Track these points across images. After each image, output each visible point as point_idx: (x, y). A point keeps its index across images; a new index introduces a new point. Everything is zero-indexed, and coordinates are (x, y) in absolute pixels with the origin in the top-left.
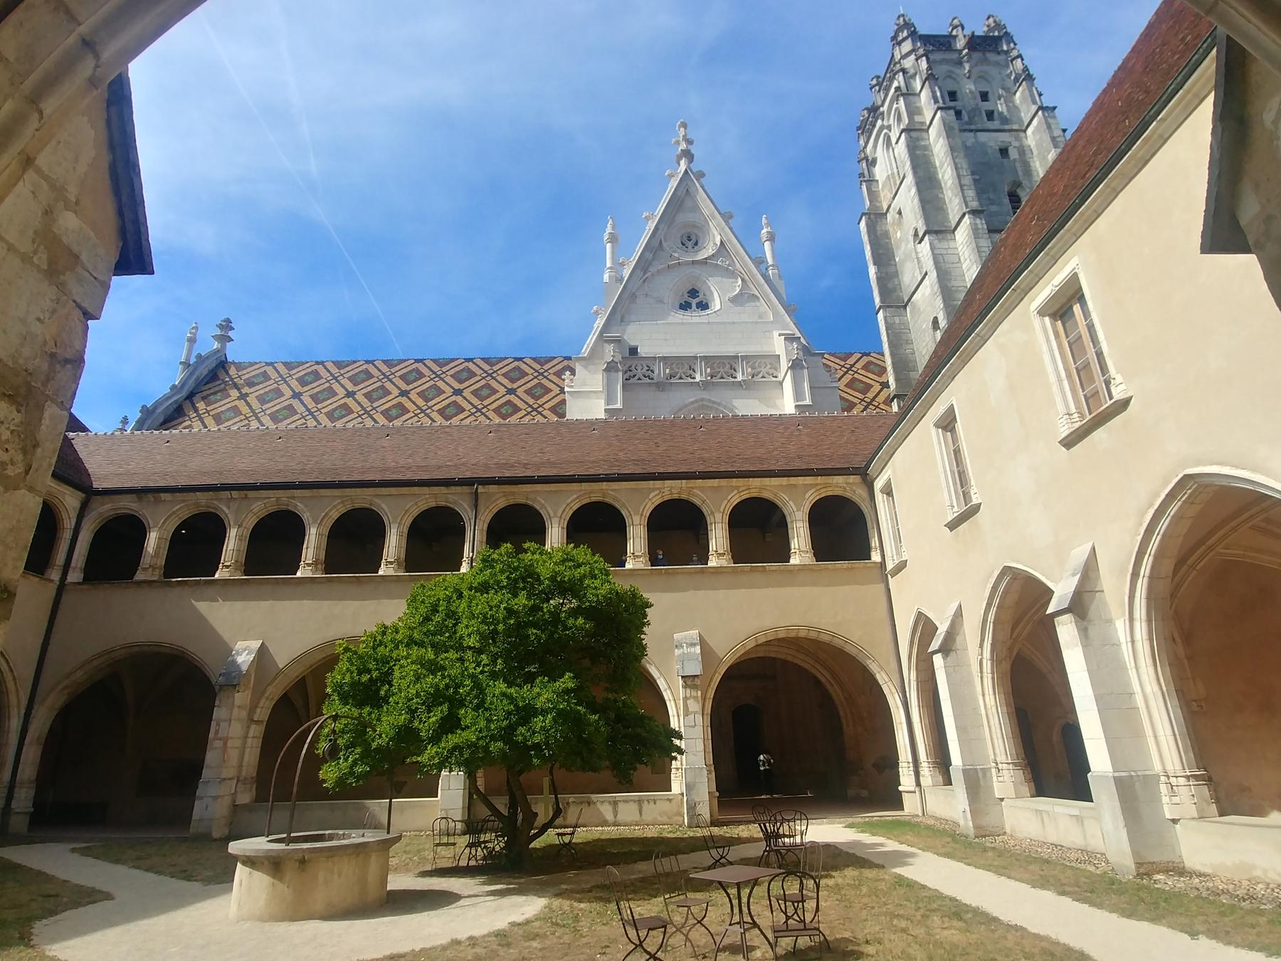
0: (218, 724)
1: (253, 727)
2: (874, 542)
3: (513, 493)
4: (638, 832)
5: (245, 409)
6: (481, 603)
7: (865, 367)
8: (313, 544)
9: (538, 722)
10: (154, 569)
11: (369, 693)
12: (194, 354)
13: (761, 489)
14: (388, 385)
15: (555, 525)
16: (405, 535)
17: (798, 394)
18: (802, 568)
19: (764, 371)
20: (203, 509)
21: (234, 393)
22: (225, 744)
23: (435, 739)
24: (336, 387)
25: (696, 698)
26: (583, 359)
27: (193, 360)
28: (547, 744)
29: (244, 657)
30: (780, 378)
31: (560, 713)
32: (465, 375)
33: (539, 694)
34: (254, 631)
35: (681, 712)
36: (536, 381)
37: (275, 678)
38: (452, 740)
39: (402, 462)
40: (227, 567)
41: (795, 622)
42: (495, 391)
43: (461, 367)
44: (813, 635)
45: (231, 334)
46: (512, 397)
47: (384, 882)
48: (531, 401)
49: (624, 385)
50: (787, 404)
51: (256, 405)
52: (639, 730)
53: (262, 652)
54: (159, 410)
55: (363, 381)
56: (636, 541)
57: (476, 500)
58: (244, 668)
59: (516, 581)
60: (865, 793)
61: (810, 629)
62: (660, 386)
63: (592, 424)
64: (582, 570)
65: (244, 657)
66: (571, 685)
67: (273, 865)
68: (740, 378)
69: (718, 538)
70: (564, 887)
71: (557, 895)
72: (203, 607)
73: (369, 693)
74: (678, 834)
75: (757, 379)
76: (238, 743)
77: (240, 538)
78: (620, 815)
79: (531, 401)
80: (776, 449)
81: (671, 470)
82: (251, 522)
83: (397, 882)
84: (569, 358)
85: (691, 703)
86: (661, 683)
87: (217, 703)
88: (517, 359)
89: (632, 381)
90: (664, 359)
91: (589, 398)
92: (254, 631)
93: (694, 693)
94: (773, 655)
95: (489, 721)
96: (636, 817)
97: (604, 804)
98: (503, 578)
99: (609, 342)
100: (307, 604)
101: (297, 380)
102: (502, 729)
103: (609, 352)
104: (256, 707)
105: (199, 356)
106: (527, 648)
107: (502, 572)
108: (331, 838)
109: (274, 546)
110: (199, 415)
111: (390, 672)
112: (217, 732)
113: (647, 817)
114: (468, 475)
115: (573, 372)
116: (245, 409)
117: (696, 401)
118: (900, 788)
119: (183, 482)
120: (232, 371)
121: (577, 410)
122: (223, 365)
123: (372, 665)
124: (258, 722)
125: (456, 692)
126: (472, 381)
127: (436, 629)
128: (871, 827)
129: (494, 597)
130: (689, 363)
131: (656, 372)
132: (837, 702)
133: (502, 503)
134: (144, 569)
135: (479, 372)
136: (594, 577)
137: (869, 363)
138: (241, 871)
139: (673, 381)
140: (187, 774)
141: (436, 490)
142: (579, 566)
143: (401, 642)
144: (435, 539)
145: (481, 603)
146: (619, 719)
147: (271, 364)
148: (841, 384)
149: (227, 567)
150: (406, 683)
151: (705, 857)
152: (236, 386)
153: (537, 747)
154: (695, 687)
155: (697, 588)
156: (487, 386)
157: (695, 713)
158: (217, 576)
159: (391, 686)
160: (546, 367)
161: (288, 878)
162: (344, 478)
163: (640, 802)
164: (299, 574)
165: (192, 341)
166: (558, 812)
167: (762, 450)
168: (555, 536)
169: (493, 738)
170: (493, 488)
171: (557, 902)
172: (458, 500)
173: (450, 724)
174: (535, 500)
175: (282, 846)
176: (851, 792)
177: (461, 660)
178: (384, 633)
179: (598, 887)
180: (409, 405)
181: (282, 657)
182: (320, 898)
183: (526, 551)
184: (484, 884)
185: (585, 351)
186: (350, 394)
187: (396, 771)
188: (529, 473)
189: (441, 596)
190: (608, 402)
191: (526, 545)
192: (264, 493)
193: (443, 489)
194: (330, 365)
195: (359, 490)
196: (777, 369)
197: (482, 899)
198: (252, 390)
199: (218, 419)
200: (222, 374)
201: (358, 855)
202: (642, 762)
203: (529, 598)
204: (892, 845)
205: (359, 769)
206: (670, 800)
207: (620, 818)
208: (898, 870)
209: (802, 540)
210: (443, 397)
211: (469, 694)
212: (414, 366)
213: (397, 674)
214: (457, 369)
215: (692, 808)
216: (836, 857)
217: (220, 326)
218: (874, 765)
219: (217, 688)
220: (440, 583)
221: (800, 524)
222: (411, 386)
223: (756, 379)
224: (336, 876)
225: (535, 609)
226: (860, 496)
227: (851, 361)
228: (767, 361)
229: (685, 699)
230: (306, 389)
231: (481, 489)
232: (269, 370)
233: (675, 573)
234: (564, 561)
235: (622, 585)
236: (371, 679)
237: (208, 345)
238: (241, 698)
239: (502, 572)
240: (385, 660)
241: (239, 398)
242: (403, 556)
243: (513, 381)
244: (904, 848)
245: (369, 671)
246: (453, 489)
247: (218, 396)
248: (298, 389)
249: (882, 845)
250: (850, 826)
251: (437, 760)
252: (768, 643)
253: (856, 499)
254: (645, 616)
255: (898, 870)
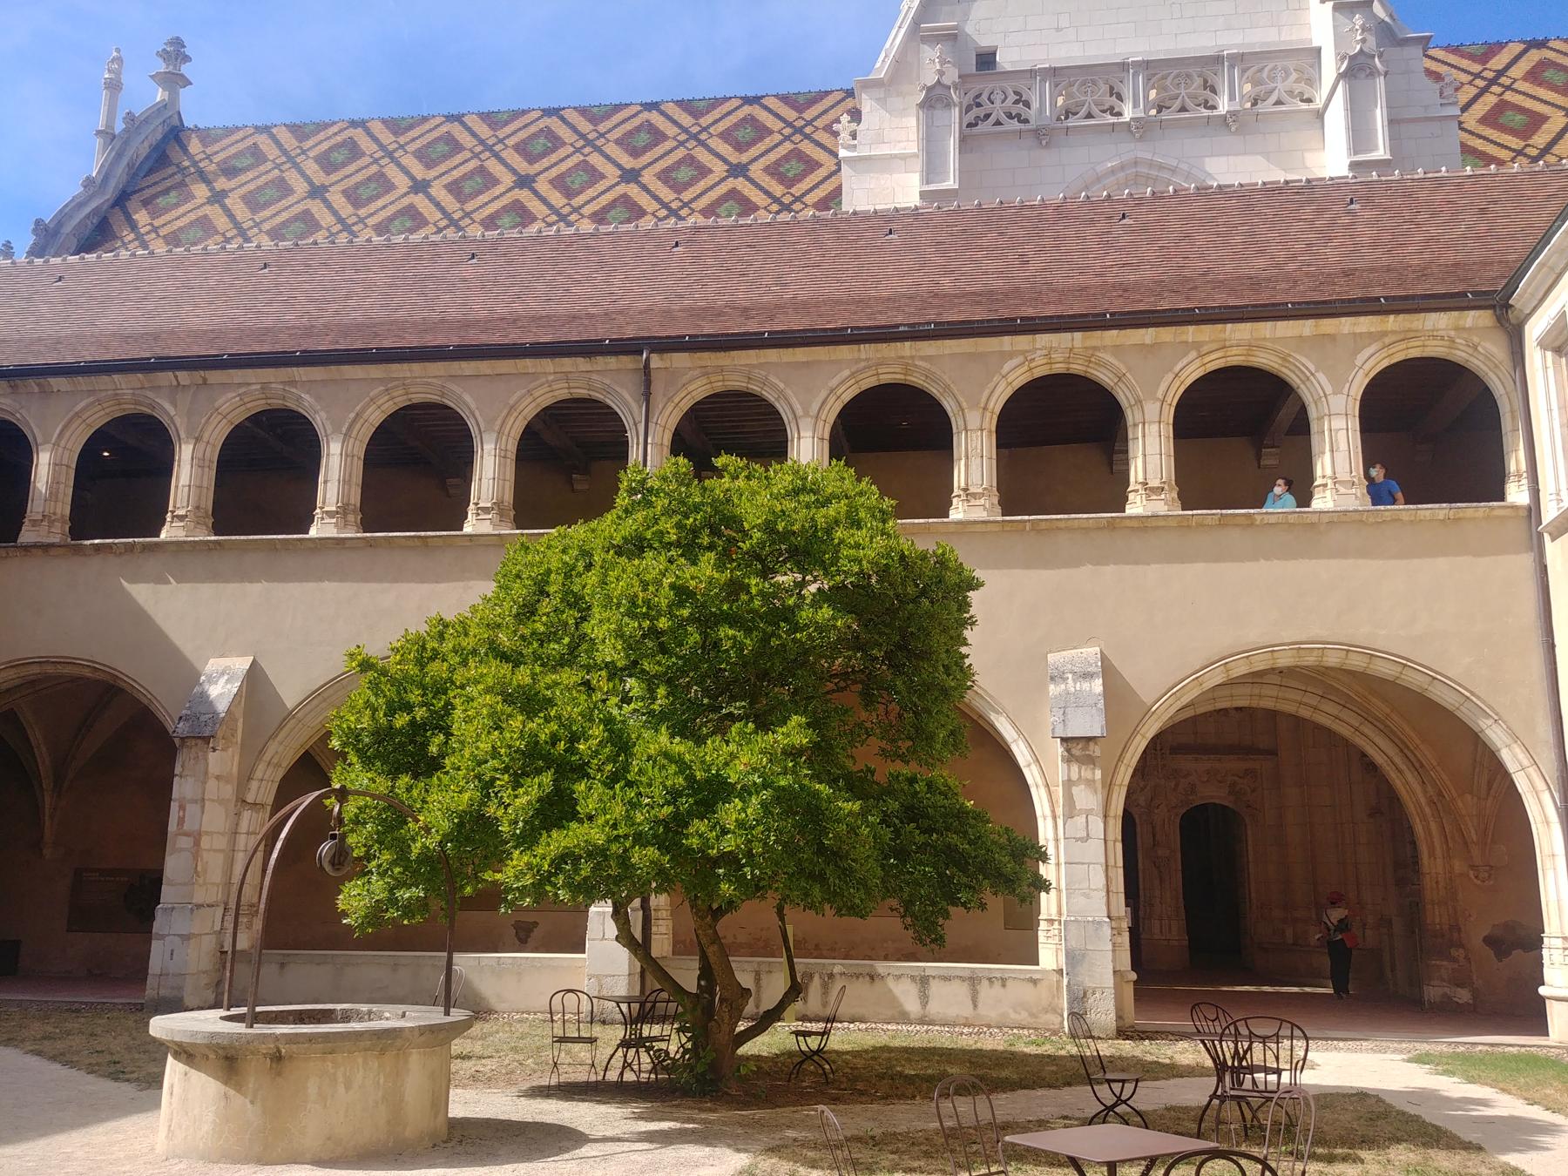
0: (182, 808)
1: (247, 814)
2: (1516, 461)
3: (721, 370)
4: (966, 1040)
5: (222, 222)
6: (624, 579)
7: (1534, 75)
8: (337, 474)
9: (730, 812)
10: (51, 523)
11: (409, 750)
12: (120, 115)
13: (1250, 346)
14: (493, 166)
15: (807, 434)
16: (512, 455)
17: (1359, 135)
18: (1338, 519)
19: (1281, 87)
20: (130, 408)
21: (201, 191)
22: (197, 843)
23: (528, 839)
24: (392, 171)
25: (1090, 783)
26: (878, 84)
27: (119, 126)
28: (749, 854)
29: (221, 685)
30: (1319, 103)
31: (782, 796)
32: (643, 138)
33: (733, 756)
34: (251, 638)
35: (1060, 811)
36: (788, 146)
37: (281, 727)
38: (557, 841)
39: (501, 310)
40: (181, 518)
41: (1317, 630)
42: (704, 171)
43: (636, 122)
44: (1357, 662)
45: (185, 69)
46: (740, 184)
47: (440, 1101)
48: (778, 190)
49: (963, 140)
50: (1331, 159)
51: (241, 212)
52: (954, 839)
53: (255, 678)
54: (68, 228)
55: (445, 157)
56: (974, 462)
57: (648, 383)
58: (222, 707)
59: (695, 532)
60: (1463, 996)
61: (1349, 648)
62: (1042, 136)
63: (887, 221)
64: (831, 511)
65: (221, 685)
66: (801, 739)
67: (225, 1061)
68: (1224, 105)
69: (1150, 454)
70: (791, 1133)
71: (772, 1150)
72: (141, 593)
73: (409, 750)
74: (1048, 1049)
75: (1266, 107)
76: (221, 843)
77: (199, 462)
78: (928, 1003)
79: (778, 190)
80: (1294, 258)
81: (1050, 311)
82: (217, 433)
83: (465, 1104)
84: (850, 93)
85: (1079, 792)
86: (1021, 753)
87: (178, 770)
88: (747, 101)
89: (983, 127)
90: (1054, 72)
91: (890, 166)
92: (251, 638)
93: (1087, 773)
94: (1268, 704)
95: (633, 805)
96: (966, 1011)
97: (901, 981)
98: (667, 525)
99: (933, 39)
100: (330, 587)
101: (317, 159)
102: (657, 822)
103: (931, 65)
104: (250, 779)
105: (130, 117)
106: (720, 670)
107: (668, 512)
108: (346, 1017)
109: (265, 476)
110: (139, 237)
111: (449, 707)
112: (181, 821)
113: (988, 1011)
114: (630, 332)
115: (856, 115)
116: (222, 222)
117: (1122, 167)
118: (1542, 991)
119: (88, 355)
120: (195, 146)
121: (865, 194)
122: (176, 134)
123: (414, 696)
124: (255, 805)
125: (571, 750)
126: (659, 150)
127: (544, 625)
128: (1468, 1066)
129: (652, 563)
130: (1105, 79)
131: (1035, 105)
132: (1411, 808)
133: (699, 390)
134: (35, 523)
135: (671, 130)
136: (857, 524)
137: (1543, 65)
138: (173, 1069)
139: (1072, 122)
140: (139, 896)
141: (567, 364)
142: (826, 502)
143: (474, 652)
144: (570, 458)
145: (624, 579)
146: (912, 813)
147: (266, 129)
148: (1471, 119)
149: (181, 518)
150: (477, 732)
151: (1082, 1099)
152: (203, 177)
153: (729, 859)
154: (1089, 761)
155: (1099, 561)
156: (690, 160)
157: (1088, 813)
158: (163, 535)
159: (448, 735)
160: (808, 115)
161: (251, 1084)
162: (387, 344)
163: (973, 981)
164: (313, 532)
165: (114, 86)
166: (795, 990)
167: (1261, 262)
168: (807, 447)
169: (639, 839)
170: (680, 360)
171: (767, 1163)
172: (610, 382)
173: (557, 810)
174: (764, 382)
175: (239, 1028)
176: (1433, 992)
177: (588, 686)
178: (441, 637)
179: (858, 1139)
180: (535, 206)
181: (291, 692)
182: (312, 1125)
183: (719, 473)
184: (640, 1117)
185: (881, 67)
186: (420, 187)
187: (461, 905)
188: (752, 327)
189: (554, 565)
190: (927, 180)
191: (719, 462)
192: (237, 375)
193: (582, 364)
194: (377, 127)
195: (416, 368)
196: (1313, 81)
197: (626, 1146)
198: (233, 184)
199: (173, 240)
200: (175, 153)
201: (383, 1052)
202: (955, 901)
203: (720, 566)
204: (1508, 1105)
205: (405, 894)
206: (1035, 982)
207: (934, 1008)
208: (1513, 1159)
209: (1341, 458)
210: (600, 186)
211: (597, 753)
212: (541, 124)
213: (458, 713)
214: (628, 126)
215: (1079, 999)
216: (1372, 1120)
217: (164, 55)
218: (1489, 941)
219: (177, 741)
220: (555, 544)
221: (1338, 423)
222: (537, 167)
223: (1261, 108)
224: (341, 1089)
225: (735, 588)
226: (1488, 357)
227: (1498, 62)
228: (1291, 64)
229: (1069, 784)
230: (334, 177)
231: (656, 361)
232: (263, 141)
233: (1054, 529)
234: (796, 492)
235: (917, 536)
236: (413, 722)
237: (144, 94)
238: (222, 761)
239: (668, 512)
240: (440, 689)
241: (210, 202)
242: (509, 497)
243: (740, 147)
244: (1537, 1113)
245: (408, 707)
246: (602, 362)
247: (173, 197)
248: (319, 178)
249: (1484, 1103)
250: (1420, 1059)
251: (528, 880)
252: (1256, 678)
253: (1477, 364)
254: (964, 605)
255: (1513, 1159)
